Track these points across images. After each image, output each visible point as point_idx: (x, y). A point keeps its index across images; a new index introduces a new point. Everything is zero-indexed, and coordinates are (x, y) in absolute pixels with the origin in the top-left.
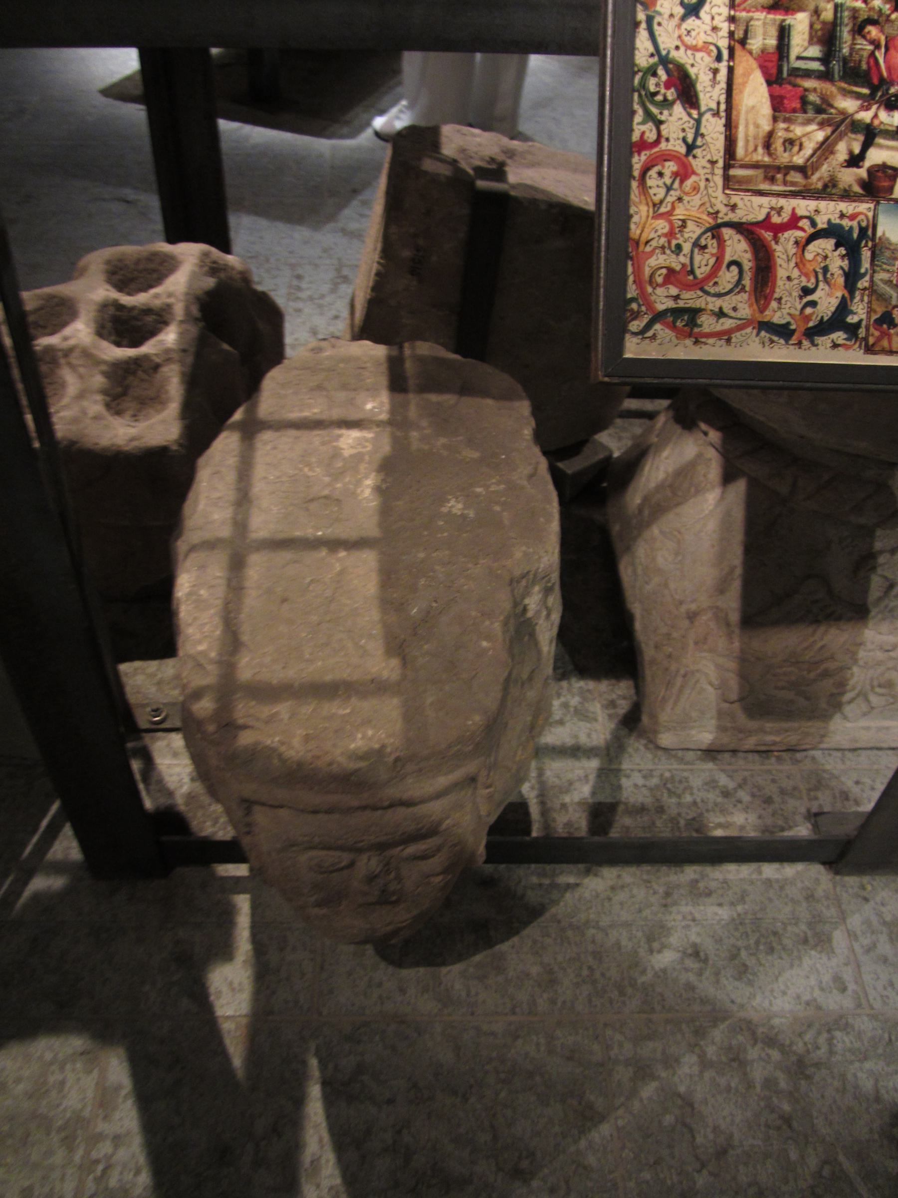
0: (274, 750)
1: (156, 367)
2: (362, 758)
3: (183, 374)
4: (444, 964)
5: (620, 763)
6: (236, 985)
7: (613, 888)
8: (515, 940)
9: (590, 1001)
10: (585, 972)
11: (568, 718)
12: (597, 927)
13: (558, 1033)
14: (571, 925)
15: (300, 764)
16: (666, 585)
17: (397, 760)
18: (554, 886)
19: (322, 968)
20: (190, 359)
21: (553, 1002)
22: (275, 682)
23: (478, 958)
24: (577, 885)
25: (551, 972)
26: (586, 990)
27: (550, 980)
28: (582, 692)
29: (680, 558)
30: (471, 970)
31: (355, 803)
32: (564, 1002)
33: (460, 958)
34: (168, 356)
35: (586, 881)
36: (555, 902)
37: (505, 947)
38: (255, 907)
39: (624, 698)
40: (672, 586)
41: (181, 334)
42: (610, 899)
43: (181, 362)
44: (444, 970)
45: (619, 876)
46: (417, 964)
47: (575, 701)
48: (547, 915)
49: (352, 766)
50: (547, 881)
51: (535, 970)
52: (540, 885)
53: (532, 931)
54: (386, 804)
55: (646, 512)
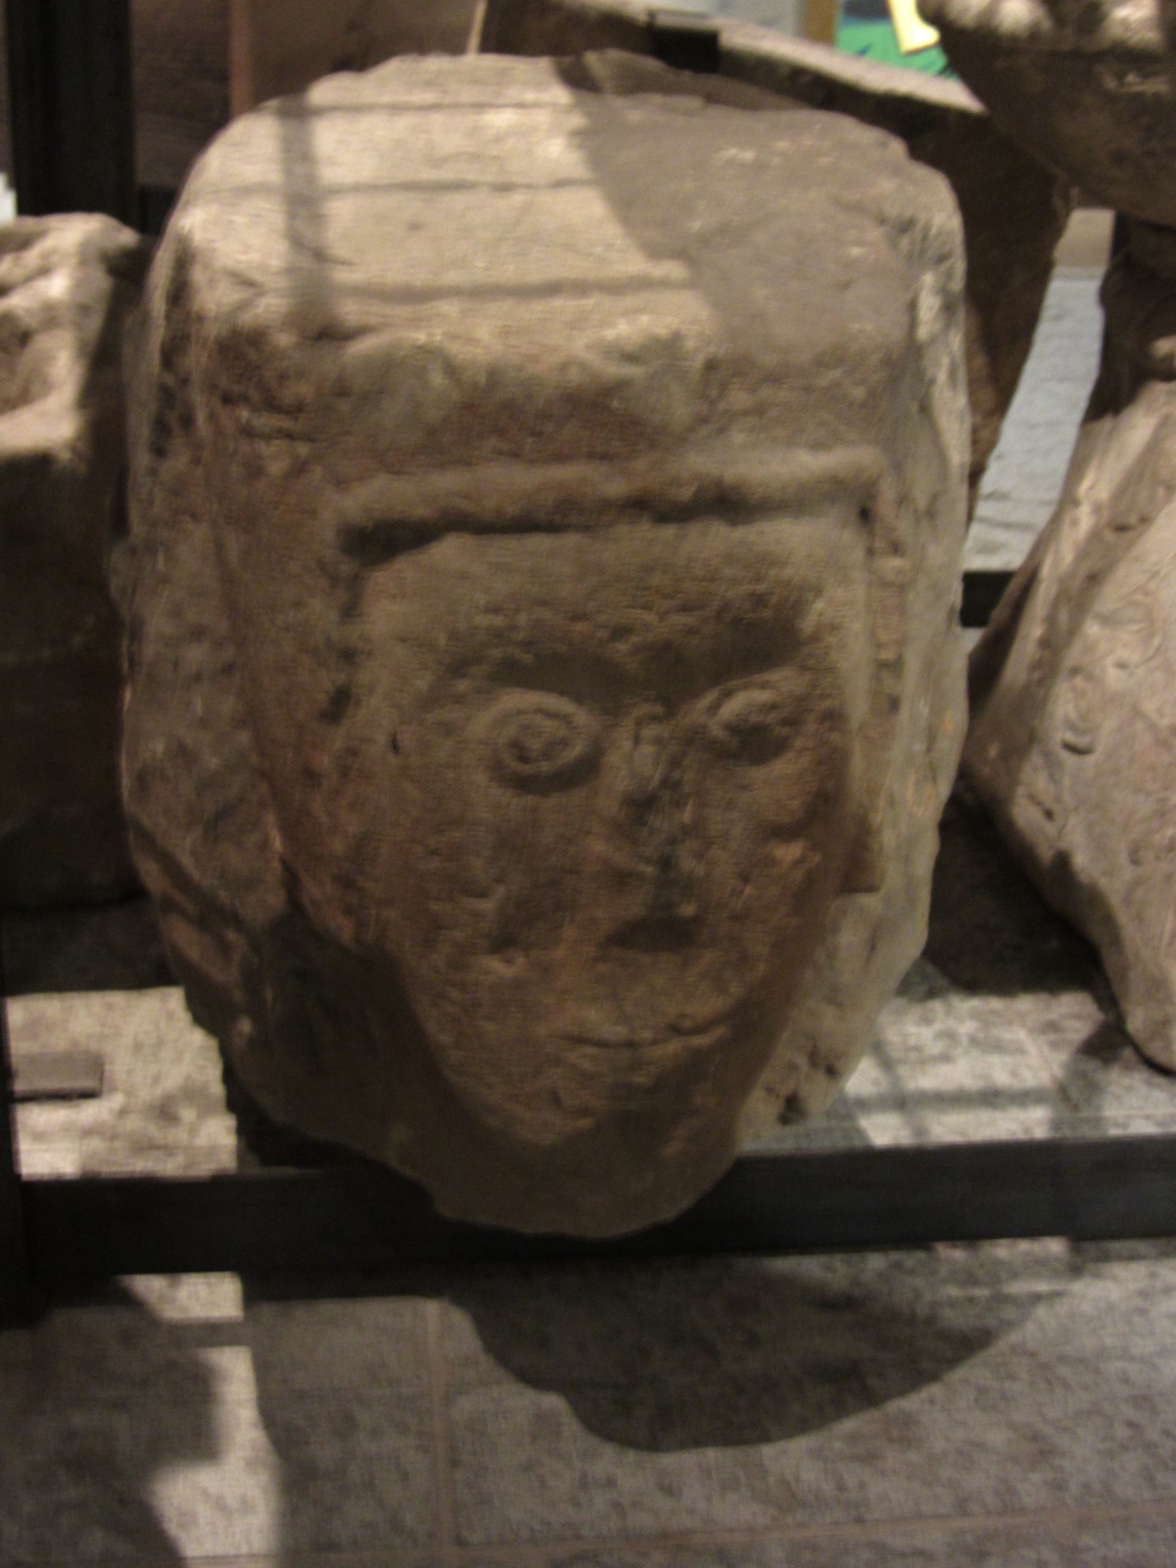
0: (427, 351)
1: (24, 338)
2: (630, 358)
3: (82, 350)
4: (766, 1438)
5: (1099, 1108)
6: (232, 1501)
7: (1144, 1294)
8: (935, 1390)
9: (1150, 1479)
10: (1121, 1432)
11: (958, 1051)
12: (1126, 1355)
13: (1086, 1540)
14: (1063, 1359)
15: (495, 375)
16: (1137, 712)
17: (711, 366)
18: (1001, 1299)
19: (455, 1463)
20: (95, 323)
21: (1058, 1486)
22: (418, 283)
23: (848, 1425)
24: (1055, 1295)
25: (1035, 1437)
26: (1132, 1462)
27: (1040, 1451)
28: (975, 1015)
29: (1156, 641)
30: (838, 1445)
31: (616, 488)
32: (1086, 1487)
33: (802, 1427)
34: (50, 316)
35: (1078, 1287)
36: (1009, 1325)
37: (910, 1403)
38: (262, 1369)
39: (1078, 1017)
40: (1149, 707)
41: (78, 285)
42: (1142, 1312)
43: (78, 326)
44: (768, 1451)
45: (1153, 1275)
46: (699, 1442)
47: (967, 1028)
48: (1001, 1345)
49: (615, 370)
50: (981, 1292)
51: (997, 1437)
52: (971, 1300)
53: (972, 1373)
54: (686, 494)
55: (1063, 618)
